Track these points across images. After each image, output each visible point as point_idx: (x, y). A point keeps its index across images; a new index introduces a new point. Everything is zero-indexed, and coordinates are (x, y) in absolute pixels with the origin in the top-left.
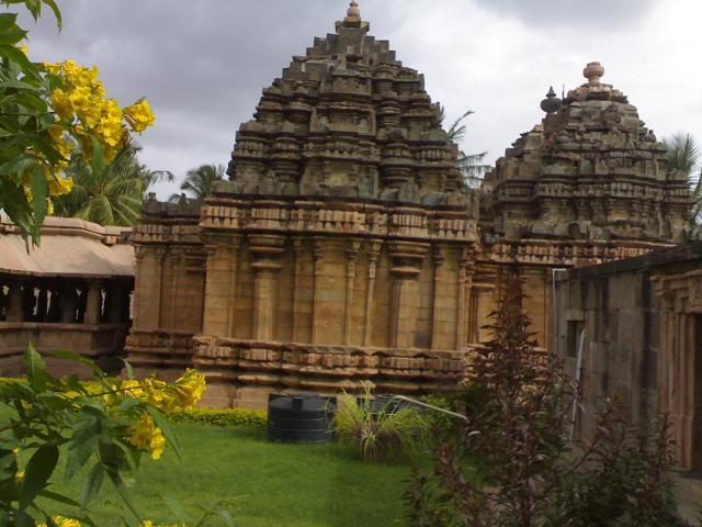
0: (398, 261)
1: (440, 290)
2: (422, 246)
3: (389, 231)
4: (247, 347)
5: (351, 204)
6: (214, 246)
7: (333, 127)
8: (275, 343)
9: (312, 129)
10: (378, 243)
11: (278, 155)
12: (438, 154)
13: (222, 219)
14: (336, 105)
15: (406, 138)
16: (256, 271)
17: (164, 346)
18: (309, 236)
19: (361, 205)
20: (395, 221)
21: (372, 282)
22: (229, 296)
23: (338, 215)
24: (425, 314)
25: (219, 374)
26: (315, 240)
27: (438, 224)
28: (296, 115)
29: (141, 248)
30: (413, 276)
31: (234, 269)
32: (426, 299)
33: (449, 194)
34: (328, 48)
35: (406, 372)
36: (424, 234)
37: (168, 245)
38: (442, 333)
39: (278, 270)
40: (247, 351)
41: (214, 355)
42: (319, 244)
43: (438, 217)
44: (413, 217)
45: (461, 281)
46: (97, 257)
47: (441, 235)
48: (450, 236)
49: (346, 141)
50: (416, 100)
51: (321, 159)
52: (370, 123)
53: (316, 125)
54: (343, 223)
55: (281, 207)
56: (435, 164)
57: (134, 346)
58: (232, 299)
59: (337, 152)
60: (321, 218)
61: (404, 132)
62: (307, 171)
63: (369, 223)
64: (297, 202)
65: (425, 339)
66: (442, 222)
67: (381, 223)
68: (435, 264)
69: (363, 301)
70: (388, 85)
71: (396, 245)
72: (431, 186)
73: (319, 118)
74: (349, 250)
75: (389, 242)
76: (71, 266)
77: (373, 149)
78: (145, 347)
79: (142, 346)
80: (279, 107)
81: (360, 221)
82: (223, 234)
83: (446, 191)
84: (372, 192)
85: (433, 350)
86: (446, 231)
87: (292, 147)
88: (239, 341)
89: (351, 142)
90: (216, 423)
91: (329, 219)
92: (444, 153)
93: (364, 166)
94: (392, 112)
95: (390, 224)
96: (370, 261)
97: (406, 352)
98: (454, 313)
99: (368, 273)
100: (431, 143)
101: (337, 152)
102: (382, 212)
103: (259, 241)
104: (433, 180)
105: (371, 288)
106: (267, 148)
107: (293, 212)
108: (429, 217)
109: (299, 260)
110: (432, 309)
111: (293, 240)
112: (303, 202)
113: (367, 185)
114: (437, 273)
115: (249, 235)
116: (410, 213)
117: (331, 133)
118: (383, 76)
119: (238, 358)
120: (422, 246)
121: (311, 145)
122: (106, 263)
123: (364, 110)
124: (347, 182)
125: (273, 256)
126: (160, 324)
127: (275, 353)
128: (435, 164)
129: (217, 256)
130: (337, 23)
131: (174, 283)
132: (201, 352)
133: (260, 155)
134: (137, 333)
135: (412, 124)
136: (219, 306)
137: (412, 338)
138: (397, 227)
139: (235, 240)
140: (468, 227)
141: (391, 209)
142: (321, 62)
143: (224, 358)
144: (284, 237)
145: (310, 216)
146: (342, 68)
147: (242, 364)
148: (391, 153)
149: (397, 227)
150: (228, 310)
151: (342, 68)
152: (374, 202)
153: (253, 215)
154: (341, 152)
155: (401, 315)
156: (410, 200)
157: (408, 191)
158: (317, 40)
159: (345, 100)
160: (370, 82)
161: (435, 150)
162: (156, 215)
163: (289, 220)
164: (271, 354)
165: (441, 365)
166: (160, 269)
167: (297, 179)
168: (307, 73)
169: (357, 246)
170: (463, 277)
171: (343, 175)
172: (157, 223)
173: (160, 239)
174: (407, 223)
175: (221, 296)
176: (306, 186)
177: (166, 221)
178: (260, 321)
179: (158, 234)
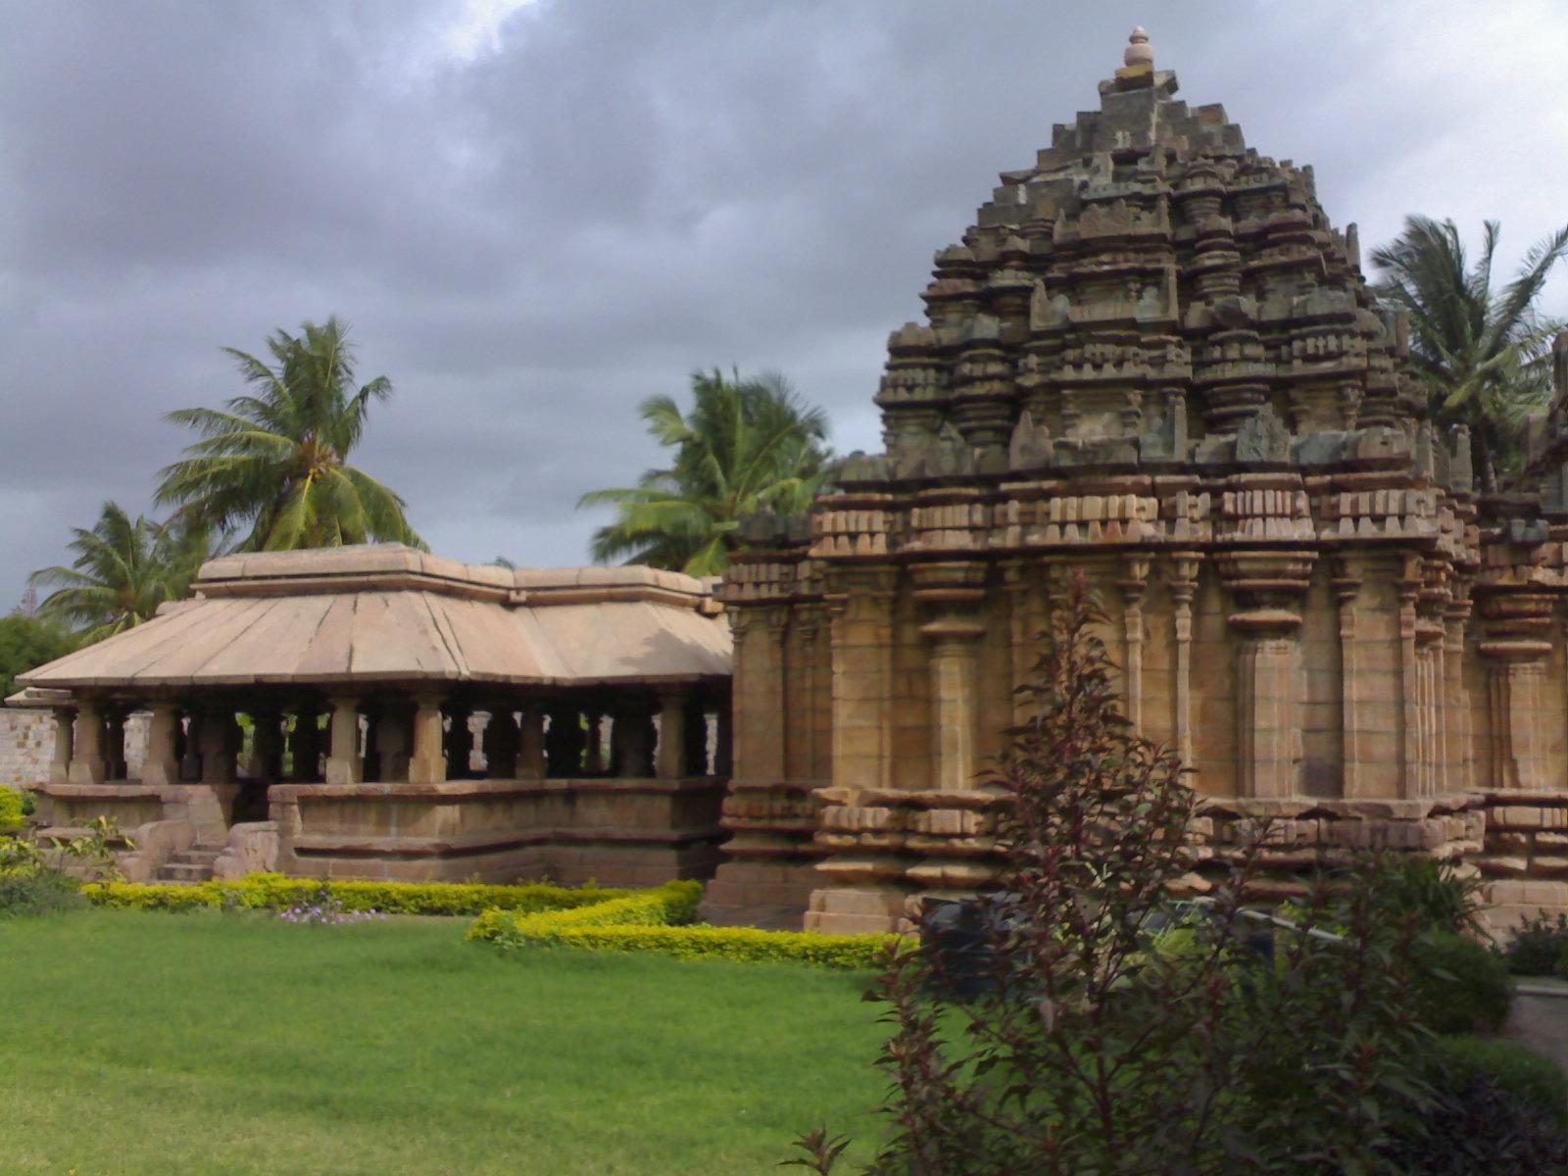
0: (1247, 599)
1: (1354, 658)
2: (1296, 560)
3: (1217, 530)
4: (920, 805)
5: (1119, 479)
6: (845, 596)
7: (1080, 315)
8: (979, 795)
9: (1036, 324)
10: (1192, 561)
11: (966, 391)
12: (1332, 343)
13: (853, 537)
14: (1088, 266)
15: (1253, 316)
16: (932, 642)
17: (796, 816)
18: (1033, 558)
19: (1147, 480)
20: (1229, 507)
21: (1184, 651)
22: (880, 699)
23: (1093, 506)
24: (1323, 715)
25: (868, 866)
26: (1047, 566)
27: (1337, 506)
28: (1007, 300)
29: (740, 613)
30: (1284, 630)
31: (886, 640)
32: (1324, 681)
33: (1363, 431)
34: (1079, 142)
35: (1280, 855)
36: (1303, 530)
37: (791, 603)
38: (1368, 759)
39: (977, 638)
40: (922, 816)
41: (855, 826)
42: (1055, 573)
43: (1335, 488)
44: (1270, 494)
45: (1404, 633)
46: (679, 641)
47: (1346, 529)
48: (1368, 530)
49: (1105, 340)
50: (1276, 228)
51: (1056, 387)
52: (1164, 295)
53: (1043, 317)
54: (1104, 523)
55: (972, 501)
56: (1328, 366)
57: (739, 817)
58: (887, 705)
59: (1088, 367)
60: (1056, 516)
61: (1248, 304)
62: (1027, 417)
63: (1168, 516)
64: (1004, 487)
65: (1326, 775)
66: (1345, 500)
67: (1197, 514)
68: (1338, 601)
69: (1165, 696)
70: (1213, 203)
71: (1235, 561)
72: (1324, 421)
73: (1050, 298)
74: (1124, 581)
75: (1216, 556)
76: (625, 661)
77: (1172, 352)
78: (759, 818)
79: (752, 817)
80: (968, 286)
81: (1144, 516)
82: (857, 569)
83: (1359, 426)
84: (1170, 447)
85: (1346, 801)
86: (1356, 519)
87: (994, 368)
88: (905, 793)
89: (1119, 341)
90: (834, 965)
91: (1072, 516)
92: (1346, 341)
93: (1154, 392)
94: (1218, 262)
95: (1218, 517)
96: (1177, 603)
97: (1278, 806)
98: (1393, 710)
99: (1175, 631)
100: (1314, 320)
101: (1088, 367)
102: (1196, 491)
103: (930, 577)
104: (1325, 405)
105: (1184, 662)
106: (945, 378)
107: (999, 508)
108: (1312, 492)
109: (1018, 611)
110: (1338, 703)
111: (1002, 570)
112: (1016, 486)
113: (1160, 432)
114: (1345, 618)
115: (910, 567)
116: (1263, 486)
117: (1074, 327)
118: (1198, 185)
119: (907, 832)
120: (1296, 560)
121: (1033, 360)
122: (696, 653)
123: (1150, 266)
124: (1115, 432)
125: (966, 608)
126: (788, 768)
127: (980, 818)
128: (1328, 366)
129: (851, 615)
130: (1101, 84)
131: (808, 683)
132: (828, 821)
133: (929, 394)
134: (744, 791)
135: (1271, 283)
136: (862, 723)
137: (1294, 774)
138: (1234, 519)
139: (883, 580)
140: (1411, 506)
141: (1221, 481)
142: (1061, 176)
143: (877, 832)
144: (984, 565)
145: (1033, 513)
146: (1102, 183)
147: (913, 843)
148: (1217, 353)
149: (1234, 519)
150: (880, 728)
151: (1102, 183)
152: (1181, 469)
153: (915, 523)
154: (1097, 367)
155: (1261, 723)
156: (1265, 457)
157: (1260, 435)
158: (1058, 131)
159: (1104, 250)
160: (1164, 204)
161: (1325, 334)
162: (767, 544)
163: (993, 526)
164: (972, 821)
165: (1366, 834)
166: (779, 656)
167: (1005, 436)
168: (1031, 206)
169: (1140, 571)
170: (1409, 625)
171: (1107, 417)
172: (769, 560)
173: (775, 593)
174: (1258, 510)
175: (864, 700)
176: (1024, 449)
177: (785, 553)
178: (945, 749)
179: (770, 583)
